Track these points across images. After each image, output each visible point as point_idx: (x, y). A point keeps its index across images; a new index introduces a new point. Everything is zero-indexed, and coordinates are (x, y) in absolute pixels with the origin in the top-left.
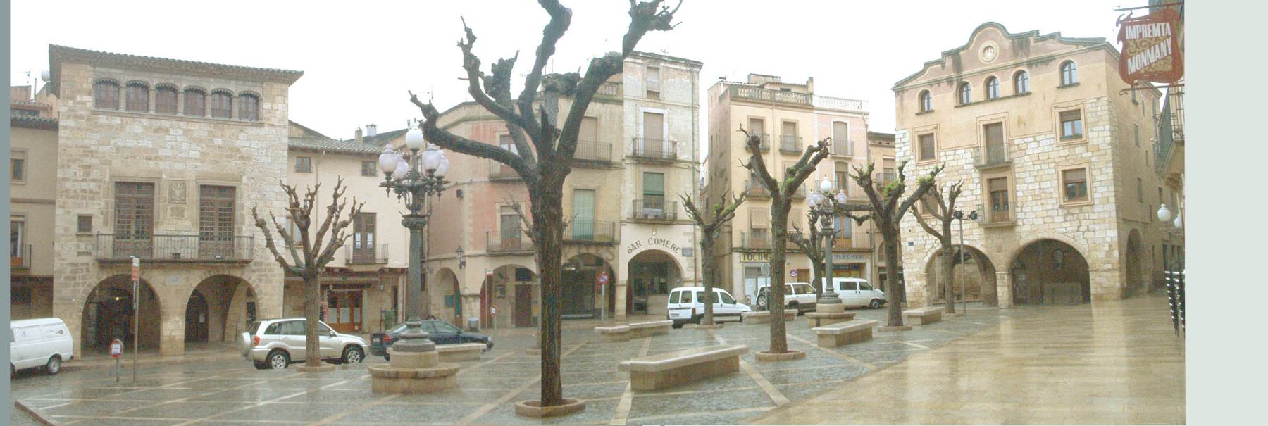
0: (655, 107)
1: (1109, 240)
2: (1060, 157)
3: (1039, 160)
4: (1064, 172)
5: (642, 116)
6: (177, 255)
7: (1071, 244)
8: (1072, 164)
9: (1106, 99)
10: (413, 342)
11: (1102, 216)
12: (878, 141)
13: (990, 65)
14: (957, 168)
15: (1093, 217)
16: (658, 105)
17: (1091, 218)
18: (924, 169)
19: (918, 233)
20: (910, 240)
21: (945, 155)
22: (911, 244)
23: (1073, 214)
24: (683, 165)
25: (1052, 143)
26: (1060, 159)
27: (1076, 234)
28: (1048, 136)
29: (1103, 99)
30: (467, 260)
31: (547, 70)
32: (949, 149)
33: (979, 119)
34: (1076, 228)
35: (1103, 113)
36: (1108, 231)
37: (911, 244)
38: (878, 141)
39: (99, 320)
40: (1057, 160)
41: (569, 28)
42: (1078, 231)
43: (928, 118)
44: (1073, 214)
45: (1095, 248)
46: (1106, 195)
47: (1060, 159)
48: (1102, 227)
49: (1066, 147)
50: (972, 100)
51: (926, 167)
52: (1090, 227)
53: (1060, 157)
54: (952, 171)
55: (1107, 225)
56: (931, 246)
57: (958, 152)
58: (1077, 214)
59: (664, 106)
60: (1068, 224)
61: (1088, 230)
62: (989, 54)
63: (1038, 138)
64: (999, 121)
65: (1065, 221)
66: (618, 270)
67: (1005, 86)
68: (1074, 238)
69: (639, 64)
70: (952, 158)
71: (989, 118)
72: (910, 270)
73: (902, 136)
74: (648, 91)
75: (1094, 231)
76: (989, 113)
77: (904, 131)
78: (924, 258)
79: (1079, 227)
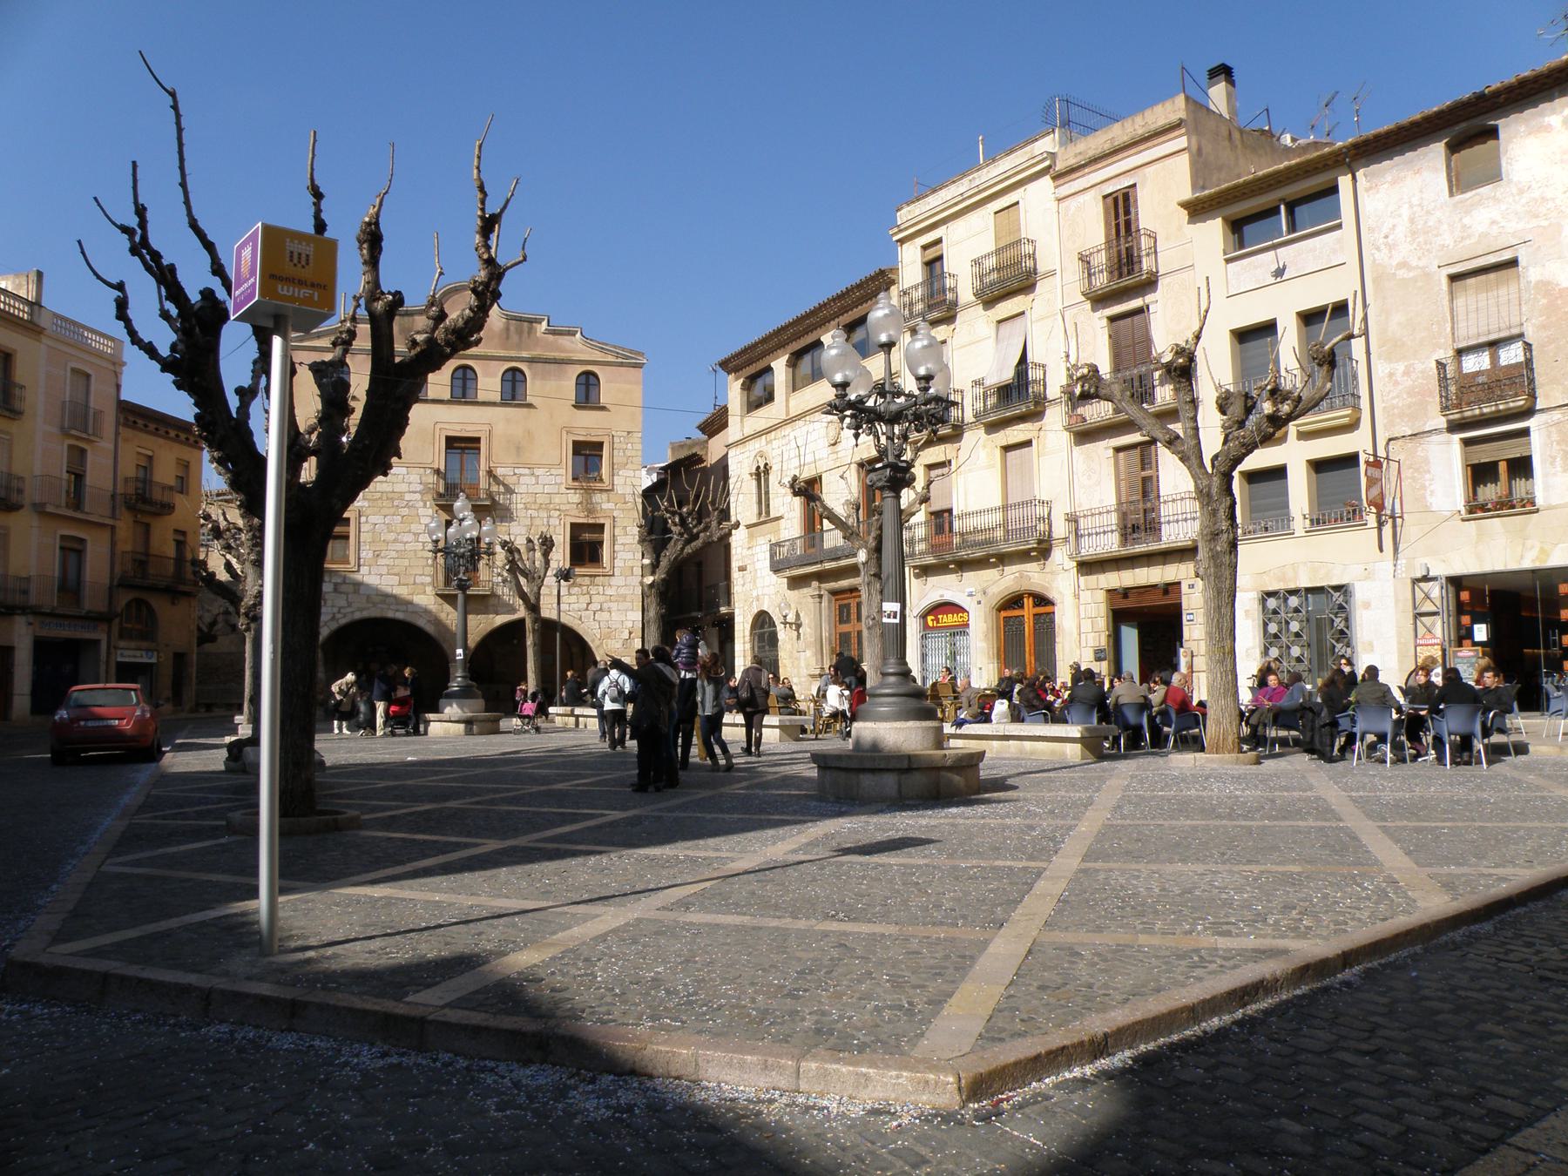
2: (569, 503)
8: (1136, 993)
9: (640, 435)
11: (622, 591)
12: (155, 426)
14: (390, 495)
15: (609, 592)
17: (606, 593)
25: (558, 481)
26: (568, 507)
27: (583, 613)
28: (554, 471)
29: (635, 435)
30: (974, 420)
31: (165, 352)
33: (438, 426)
35: (634, 453)
36: (629, 613)
38: (155, 426)
41: (130, 306)
42: (587, 609)
45: (609, 634)
46: (630, 564)
47: (568, 507)
48: (623, 606)
53: (569, 503)
56: (330, 617)
58: (588, 586)
61: (601, 610)
68: (580, 619)
71: (458, 427)
79: (588, 604)
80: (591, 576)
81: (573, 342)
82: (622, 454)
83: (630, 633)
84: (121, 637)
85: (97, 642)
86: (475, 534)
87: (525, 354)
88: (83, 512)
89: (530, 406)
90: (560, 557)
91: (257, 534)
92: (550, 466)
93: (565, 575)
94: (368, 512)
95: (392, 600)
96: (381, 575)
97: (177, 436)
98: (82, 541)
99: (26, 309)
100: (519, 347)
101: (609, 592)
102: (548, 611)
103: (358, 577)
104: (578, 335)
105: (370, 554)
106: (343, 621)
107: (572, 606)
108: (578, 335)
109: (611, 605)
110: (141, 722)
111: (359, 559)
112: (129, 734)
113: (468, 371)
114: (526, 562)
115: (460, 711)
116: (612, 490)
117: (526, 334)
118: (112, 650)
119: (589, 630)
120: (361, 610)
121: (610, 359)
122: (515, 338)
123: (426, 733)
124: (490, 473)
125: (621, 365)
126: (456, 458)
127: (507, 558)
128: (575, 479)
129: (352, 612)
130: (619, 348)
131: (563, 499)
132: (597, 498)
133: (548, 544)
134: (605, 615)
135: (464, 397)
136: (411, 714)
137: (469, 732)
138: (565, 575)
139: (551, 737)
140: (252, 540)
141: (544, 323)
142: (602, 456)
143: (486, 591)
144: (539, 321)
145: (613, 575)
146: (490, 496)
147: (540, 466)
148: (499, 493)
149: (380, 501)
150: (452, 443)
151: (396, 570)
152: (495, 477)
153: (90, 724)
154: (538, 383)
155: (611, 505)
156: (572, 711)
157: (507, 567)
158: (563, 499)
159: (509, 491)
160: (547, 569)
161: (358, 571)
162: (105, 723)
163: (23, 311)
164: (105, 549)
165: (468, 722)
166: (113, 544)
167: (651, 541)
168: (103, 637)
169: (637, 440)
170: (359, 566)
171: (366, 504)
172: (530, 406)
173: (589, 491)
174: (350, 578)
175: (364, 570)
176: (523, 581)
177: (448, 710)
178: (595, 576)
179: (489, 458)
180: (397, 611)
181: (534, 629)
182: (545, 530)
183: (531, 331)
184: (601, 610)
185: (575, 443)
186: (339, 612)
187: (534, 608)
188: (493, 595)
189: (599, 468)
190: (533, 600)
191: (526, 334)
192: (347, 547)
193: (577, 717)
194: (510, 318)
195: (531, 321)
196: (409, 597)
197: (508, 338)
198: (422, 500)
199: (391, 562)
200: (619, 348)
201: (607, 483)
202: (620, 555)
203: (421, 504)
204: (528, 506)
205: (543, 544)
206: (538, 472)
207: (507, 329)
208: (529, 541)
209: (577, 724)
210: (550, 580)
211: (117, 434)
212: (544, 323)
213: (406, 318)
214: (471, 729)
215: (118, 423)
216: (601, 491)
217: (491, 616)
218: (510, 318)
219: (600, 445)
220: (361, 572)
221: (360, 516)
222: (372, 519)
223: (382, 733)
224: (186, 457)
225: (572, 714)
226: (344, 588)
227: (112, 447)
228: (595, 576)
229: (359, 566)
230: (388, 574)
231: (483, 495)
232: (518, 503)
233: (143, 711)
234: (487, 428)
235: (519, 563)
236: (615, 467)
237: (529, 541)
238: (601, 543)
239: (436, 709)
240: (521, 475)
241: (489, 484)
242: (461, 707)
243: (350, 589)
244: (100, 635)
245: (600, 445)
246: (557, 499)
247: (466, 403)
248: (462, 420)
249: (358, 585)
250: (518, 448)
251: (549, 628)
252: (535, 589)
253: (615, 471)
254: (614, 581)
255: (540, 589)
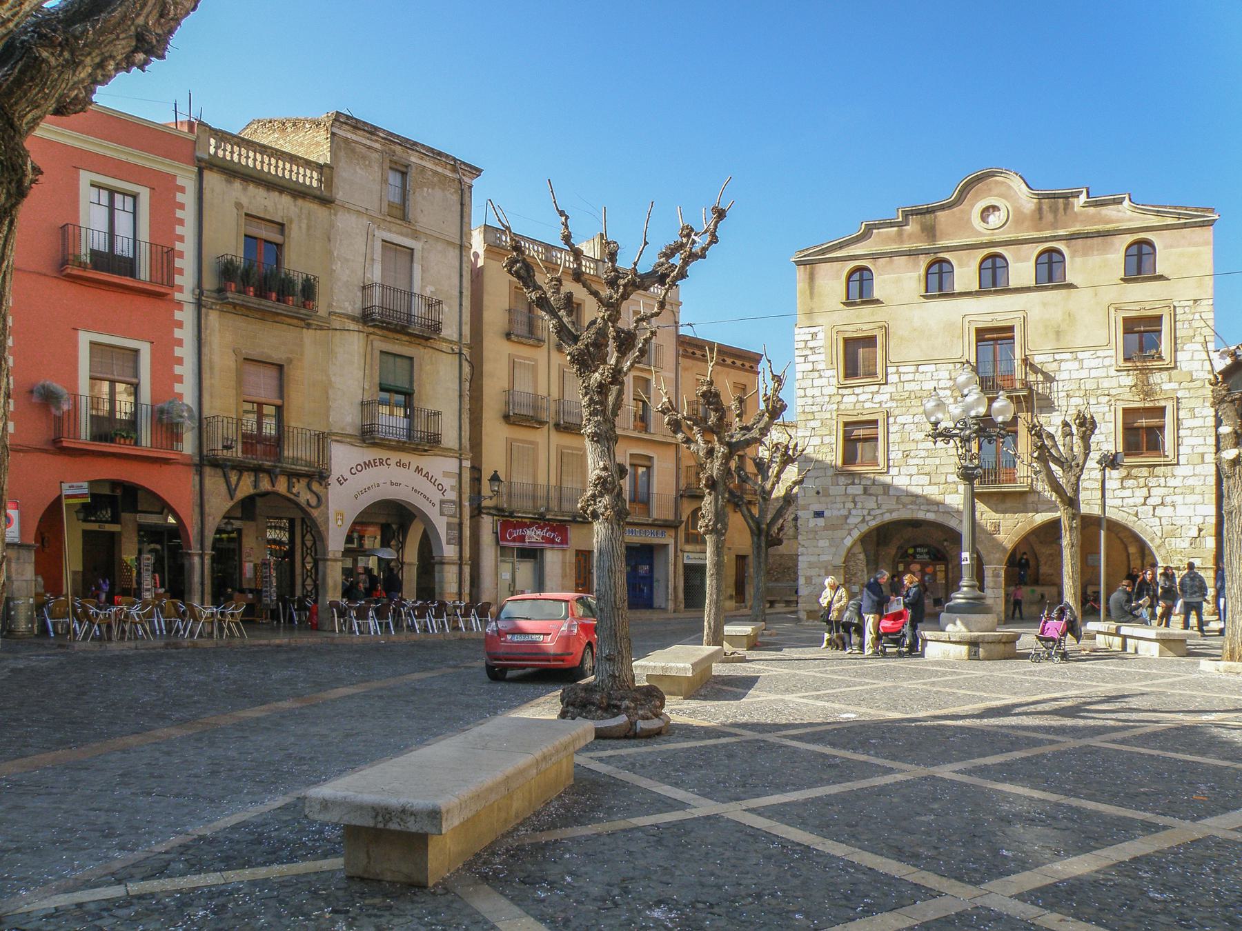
0: (401, 234)
1: (1199, 520)
2: (1120, 386)
3: (1098, 388)
4: (846, 424)
5: (378, 245)
6: (228, 182)
7: (1130, 525)
9: (1211, 302)
10: (1040, 719)
11: (1190, 482)
13: (993, 235)
15: (1171, 482)
16: (405, 230)
18: (854, 394)
19: (835, 496)
20: (817, 507)
21: (897, 372)
22: (819, 514)
23: (1136, 477)
24: (444, 346)
26: (1120, 391)
27: (1140, 509)
29: (1205, 302)
32: (906, 363)
33: (967, 319)
34: (1143, 500)
37: (819, 514)
39: (717, 603)
40: (1113, 392)
42: (1145, 504)
43: (866, 312)
44: (1136, 477)
46: (1201, 449)
47: (1120, 391)
48: (1190, 499)
49: (1131, 372)
50: (958, 288)
51: (857, 390)
52: (1168, 500)
53: (1120, 386)
54: (909, 398)
55: (1198, 498)
57: (921, 368)
59: (415, 235)
60: (1128, 493)
61: (1162, 504)
62: (995, 220)
63: (1080, 355)
64: (1009, 324)
65: (1123, 488)
66: (328, 529)
67: (1022, 269)
68: (1136, 515)
69: (375, 150)
70: (910, 377)
71: (989, 318)
72: (813, 559)
73: (809, 337)
74: (246, 236)
75: (1174, 506)
76: (993, 310)
77: (813, 330)
78: (843, 539)
79: (1146, 498)
80: (1149, 466)
81: (1119, 211)
82: (1186, 325)
83: (1200, 530)
84: (687, 541)
85: (666, 546)
86: (982, 410)
87: (1061, 232)
88: (650, 433)
89: (1070, 286)
90: (1108, 438)
91: (596, 398)
92: (1096, 348)
93: (1111, 462)
94: (897, 412)
95: (921, 500)
96: (911, 475)
97: (733, 363)
98: (650, 458)
99: (592, 266)
100: (1054, 226)
101: (1171, 482)
102: (1089, 505)
103: (887, 479)
104: (1126, 203)
105: (900, 454)
106: (873, 524)
107: (1126, 501)
108: (1126, 203)
109: (1175, 498)
110: (567, 640)
111: (888, 460)
112: (552, 652)
113: (998, 260)
114: (1061, 448)
115: (964, 629)
116: (1175, 368)
117: (1061, 210)
118: (679, 553)
119: (1147, 527)
120: (891, 511)
121: (1170, 221)
122: (1049, 217)
123: (922, 655)
124: (1026, 361)
125: (1185, 226)
126: (988, 349)
127: (1035, 444)
128: (1127, 359)
129: (882, 514)
130: (1181, 207)
131: (1114, 383)
132: (1156, 378)
133: (1087, 425)
134: (1167, 511)
135: (994, 284)
136: (907, 629)
137: (973, 656)
138: (1111, 462)
139: (1078, 670)
140: (589, 405)
141: (1083, 198)
142: (1160, 331)
143: (1023, 487)
144: (1077, 195)
145: (1178, 464)
146: (1027, 385)
147: (1084, 349)
148: (1037, 382)
149: (908, 401)
150: (983, 335)
151: (927, 469)
152: (1032, 366)
153: (516, 638)
154: (1078, 260)
155: (1174, 385)
156: (1118, 629)
157: (1036, 455)
158: (1114, 383)
159: (1049, 378)
160: (1086, 455)
161: (888, 472)
162: (530, 638)
163: (590, 267)
164: (670, 465)
165: (973, 644)
166: (678, 460)
167: (1232, 401)
168: (671, 542)
169: (1207, 308)
170: (889, 467)
171: (894, 404)
172: (1070, 286)
173: (1146, 372)
174: (878, 481)
175: (894, 471)
176: (1054, 467)
177: (950, 627)
178: (1155, 466)
179: (1025, 346)
180: (928, 511)
181: (1071, 528)
182: (1082, 408)
183: (1067, 206)
184: (1162, 504)
185: (1125, 320)
186: (869, 514)
187: (1072, 503)
188: (1032, 491)
189: (1156, 345)
190: (1070, 493)
191: (1061, 210)
192: (876, 448)
193: (1125, 638)
194: (1041, 197)
195: (1066, 197)
196: (939, 498)
197: (1041, 218)
198: (952, 396)
199: (921, 462)
200: (1181, 207)
201: (1168, 360)
202: (1186, 441)
203: (952, 400)
204: (1071, 393)
205: (1082, 425)
206: (1080, 355)
207: (1040, 209)
208: (1066, 424)
209: (1124, 647)
210: (1092, 463)
211: (677, 364)
212: (1083, 198)
213: (928, 216)
214: (976, 653)
215: (677, 356)
216: (1161, 369)
217: (1030, 514)
218: (1041, 197)
219: (1158, 319)
220: (891, 473)
221: (888, 417)
222: (900, 420)
223: (871, 652)
224: (742, 382)
225: (1117, 633)
226: (873, 490)
227: (673, 376)
228: (1155, 466)
229: (889, 467)
230: (918, 474)
231: (1018, 385)
232: (1058, 393)
233: (570, 626)
234: (1021, 315)
235: (1053, 451)
236: (1179, 341)
237: (1066, 424)
238: (1161, 428)
239: (935, 621)
240: (1062, 361)
241: (1026, 373)
242: (966, 625)
243: (880, 491)
244: (668, 539)
245: (1158, 319)
246: (1105, 384)
247: (997, 292)
248: (993, 310)
249: (887, 488)
250: (1058, 333)
251: (1089, 525)
252: (1073, 479)
253: (1179, 347)
254: (1178, 471)
255: (1078, 478)
